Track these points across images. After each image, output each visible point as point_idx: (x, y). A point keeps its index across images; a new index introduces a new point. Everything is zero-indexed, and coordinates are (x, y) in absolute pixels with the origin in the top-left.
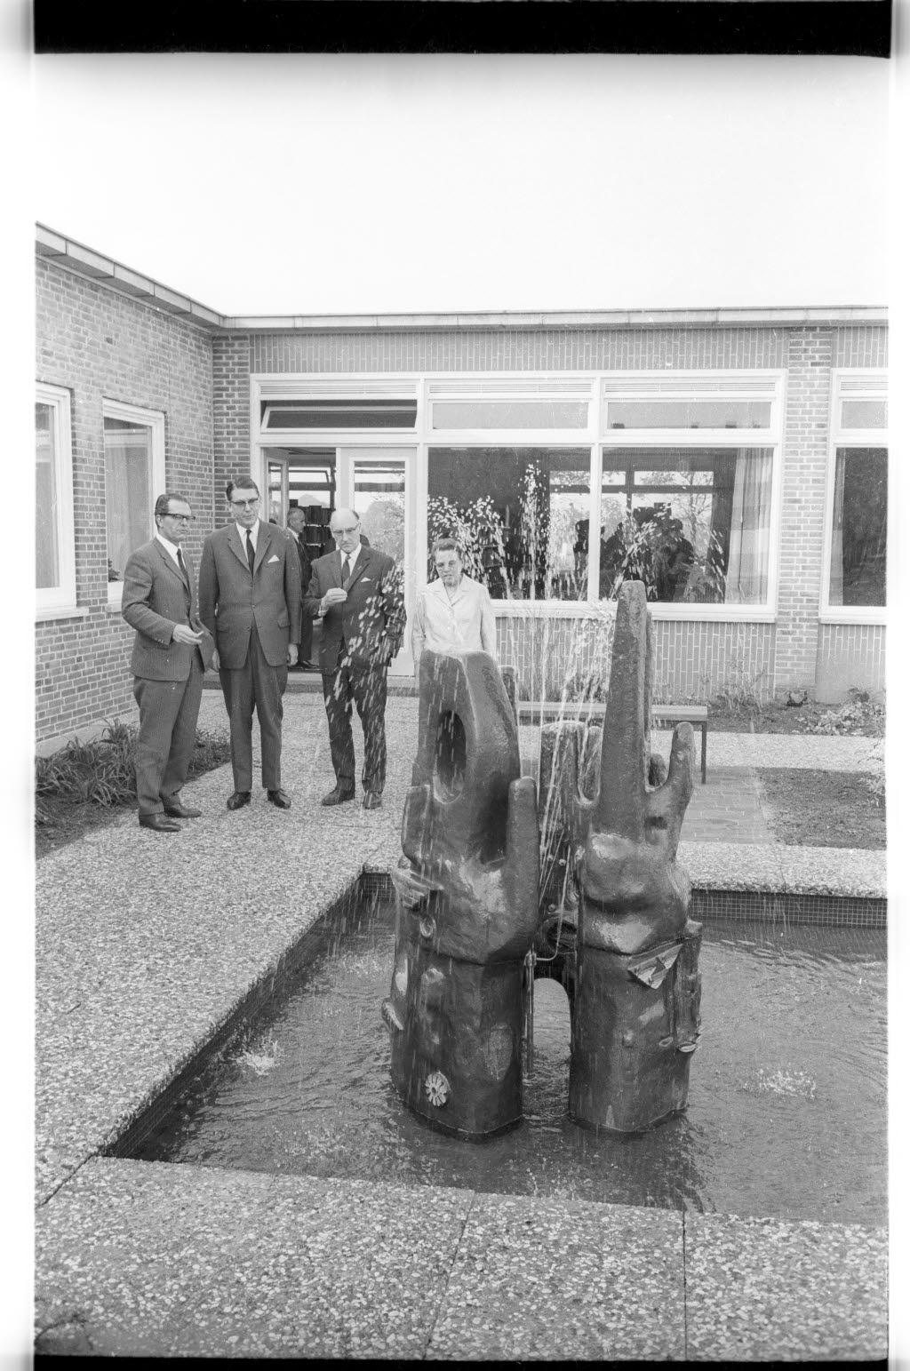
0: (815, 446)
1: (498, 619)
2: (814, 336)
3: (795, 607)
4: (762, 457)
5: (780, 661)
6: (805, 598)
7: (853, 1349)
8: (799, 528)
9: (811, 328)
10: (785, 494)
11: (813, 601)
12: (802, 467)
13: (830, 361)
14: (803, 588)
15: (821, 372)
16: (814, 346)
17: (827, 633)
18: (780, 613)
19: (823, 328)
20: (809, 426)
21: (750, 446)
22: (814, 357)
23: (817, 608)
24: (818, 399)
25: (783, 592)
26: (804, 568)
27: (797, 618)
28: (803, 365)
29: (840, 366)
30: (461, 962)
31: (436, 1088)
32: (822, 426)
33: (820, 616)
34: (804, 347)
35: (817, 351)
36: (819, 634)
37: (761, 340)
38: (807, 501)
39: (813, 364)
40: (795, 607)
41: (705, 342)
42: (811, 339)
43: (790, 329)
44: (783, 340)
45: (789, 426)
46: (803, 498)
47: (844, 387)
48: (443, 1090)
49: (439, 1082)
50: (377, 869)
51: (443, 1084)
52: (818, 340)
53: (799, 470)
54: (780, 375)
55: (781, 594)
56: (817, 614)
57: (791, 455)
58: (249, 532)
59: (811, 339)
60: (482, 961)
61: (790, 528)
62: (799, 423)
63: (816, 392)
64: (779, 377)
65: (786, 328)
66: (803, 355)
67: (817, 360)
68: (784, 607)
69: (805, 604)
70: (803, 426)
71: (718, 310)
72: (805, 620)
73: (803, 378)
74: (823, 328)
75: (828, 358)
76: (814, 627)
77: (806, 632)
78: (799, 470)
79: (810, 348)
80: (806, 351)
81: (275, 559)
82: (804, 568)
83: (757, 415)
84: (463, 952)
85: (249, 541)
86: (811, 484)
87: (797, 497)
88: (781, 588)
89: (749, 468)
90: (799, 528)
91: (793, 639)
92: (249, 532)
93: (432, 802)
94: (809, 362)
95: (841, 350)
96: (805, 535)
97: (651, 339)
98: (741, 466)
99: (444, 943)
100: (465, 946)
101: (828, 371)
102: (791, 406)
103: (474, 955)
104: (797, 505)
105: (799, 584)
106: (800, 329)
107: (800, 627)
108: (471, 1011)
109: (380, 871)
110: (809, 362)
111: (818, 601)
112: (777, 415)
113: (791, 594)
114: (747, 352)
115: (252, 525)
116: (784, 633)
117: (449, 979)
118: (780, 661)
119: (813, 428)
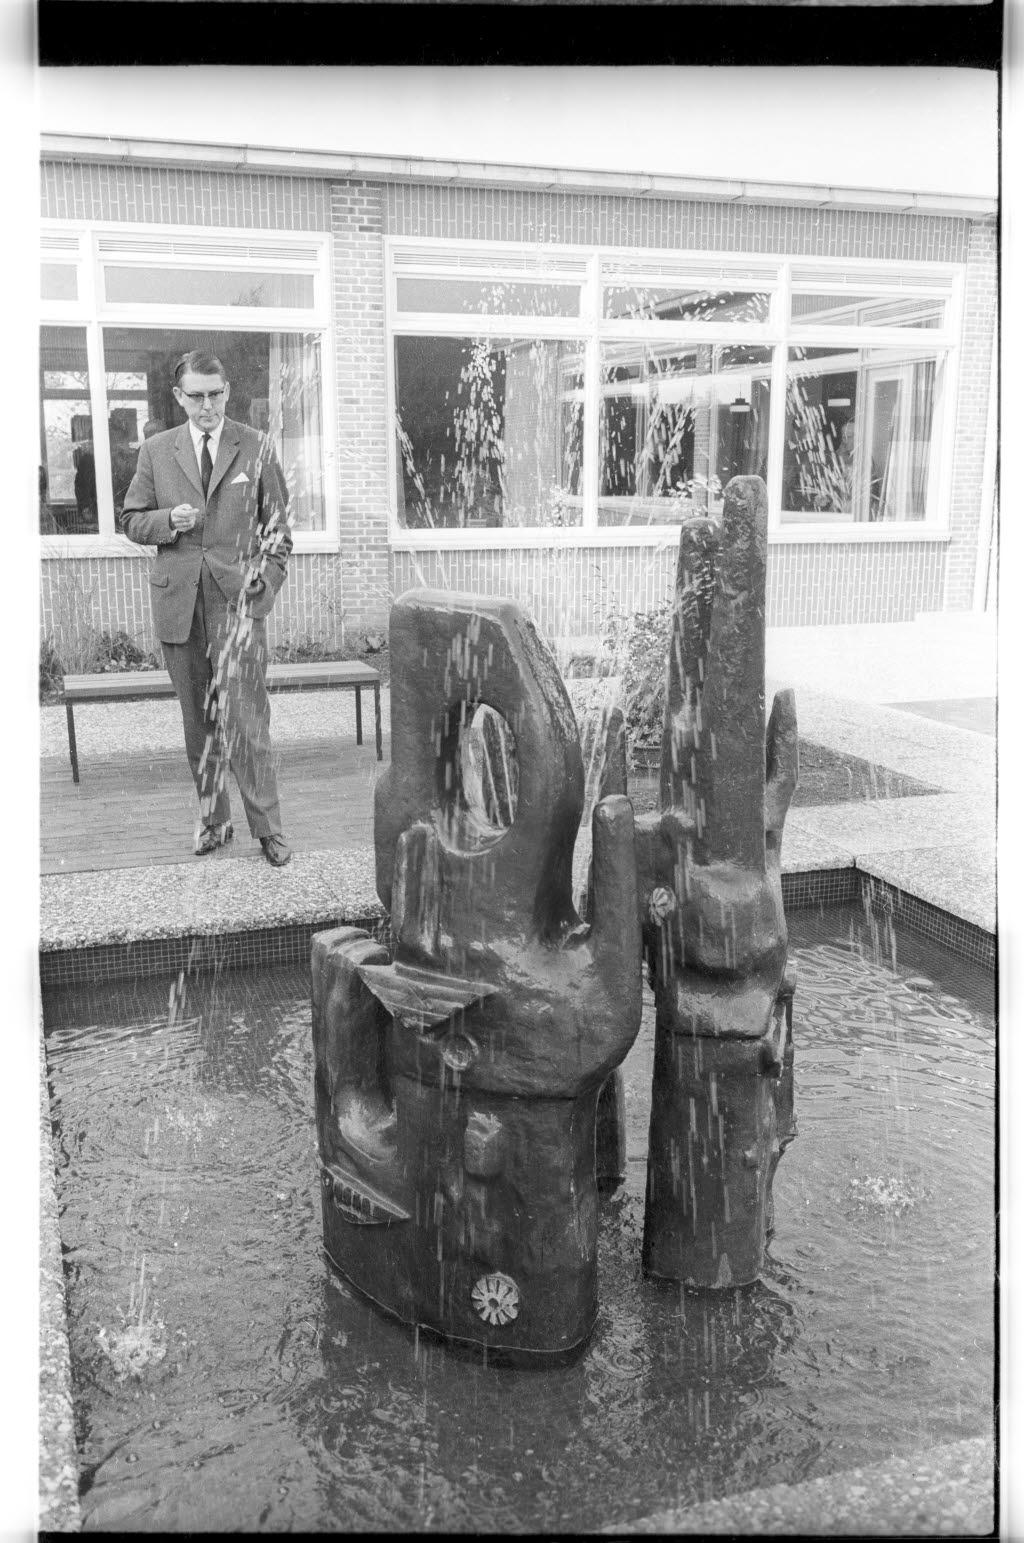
0: (370, 333)
1: (44, 561)
2: (361, 193)
3: (361, 532)
4: (302, 345)
5: (347, 599)
6: (372, 521)
7: (988, 1511)
8: (359, 435)
9: (356, 183)
10: (341, 393)
11: (381, 524)
12: (357, 359)
13: (378, 226)
14: (367, 508)
15: (371, 238)
16: (360, 204)
17: (454, 562)
18: (343, 541)
19: (370, 184)
20: (362, 307)
21: (287, 331)
22: (362, 220)
23: (386, 532)
24: (371, 273)
25: (346, 512)
26: (368, 484)
27: (364, 545)
28: (351, 228)
29: (392, 233)
30: (534, 1099)
31: (499, 1298)
32: (377, 307)
33: (390, 542)
34: (349, 205)
35: (367, 212)
36: (390, 564)
37: (263, 192)
38: (366, 401)
39: (362, 229)
40: (361, 532)
41: (176, 188)
42: (357, 196)
43: (332, 181)
44: (321, 196)
45: (339, 306)
46: (361, 398)
47: (400, 259)
48: (513, 1299)
49: (503, 1289)
50: (60, 943)
51: (510, 1290)
52: (365, 199)
53: (353, 363)
54: (323, 241)
55: (342, 517)
56: (385, 540)
57: (343, 343)
58: (207, 438)
59: (357, 196)
60: (571, 1092)
61: (351, 435)
62: (351, 302)
63: (367, 265)
64: (322, 243)
65: (326, 180)
66: (349, 216)
67: (366, 224)
68: (349, 533)
69: (372, 527)
70: (355, 306)
71: (245, 148)
72: (375, 548)
73: (352, 246)
74: (370, 184)
75: (378, 221)
76: (384, 556)
77: (375, 562)
78: (353, 363)
79: (356, 207)
80: (351, 211)
81: (242, 478)
82: (368, 484)
83: (297, 290)
84: (540, 1084)
85: (206, 453)
86: (369, 379)
87: (354, 396)
88: (343, 509)
89: (285, 359)
90: (359, 435)
91: (362, 572)
92: (207, 438)
93: (441, 853)
94: (357, 225)
95: (392, 213)
96: (367, 443)
97: (138, 181)
98: (275, 354)
99: (504, 1072)
100: (545, 1075)
101: (379, 238)
102: (339, 282)
103: (557, 1086)
104: (354, 406)
105: (364, 503)
106: (342, 182)
107: (367, 556)
108: (558, 1172)
109: (64, 946)
110: (357, 225)
111: (386, 525)
112: (323, 289)
113: (355, 517)
114: (312, 209)
115: (212, 429)
116: (351, 565)
117: (510, 1129)
118: (347, 599)
119: (367, 309)
